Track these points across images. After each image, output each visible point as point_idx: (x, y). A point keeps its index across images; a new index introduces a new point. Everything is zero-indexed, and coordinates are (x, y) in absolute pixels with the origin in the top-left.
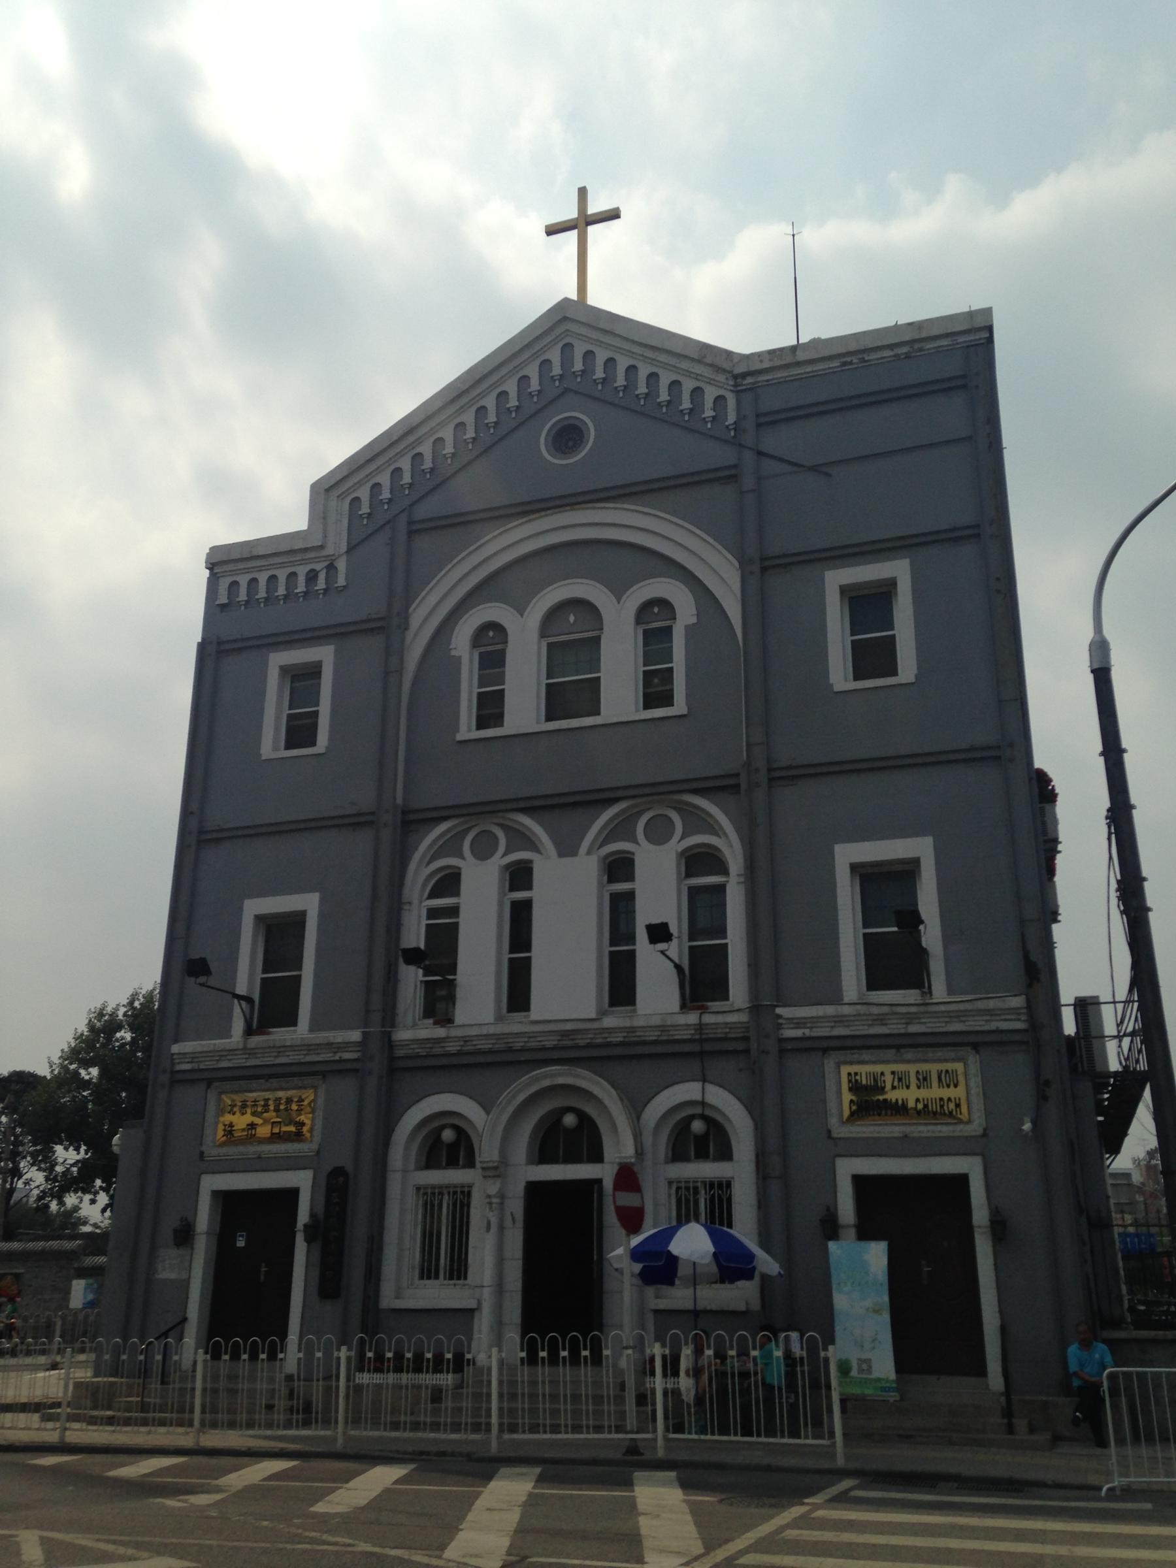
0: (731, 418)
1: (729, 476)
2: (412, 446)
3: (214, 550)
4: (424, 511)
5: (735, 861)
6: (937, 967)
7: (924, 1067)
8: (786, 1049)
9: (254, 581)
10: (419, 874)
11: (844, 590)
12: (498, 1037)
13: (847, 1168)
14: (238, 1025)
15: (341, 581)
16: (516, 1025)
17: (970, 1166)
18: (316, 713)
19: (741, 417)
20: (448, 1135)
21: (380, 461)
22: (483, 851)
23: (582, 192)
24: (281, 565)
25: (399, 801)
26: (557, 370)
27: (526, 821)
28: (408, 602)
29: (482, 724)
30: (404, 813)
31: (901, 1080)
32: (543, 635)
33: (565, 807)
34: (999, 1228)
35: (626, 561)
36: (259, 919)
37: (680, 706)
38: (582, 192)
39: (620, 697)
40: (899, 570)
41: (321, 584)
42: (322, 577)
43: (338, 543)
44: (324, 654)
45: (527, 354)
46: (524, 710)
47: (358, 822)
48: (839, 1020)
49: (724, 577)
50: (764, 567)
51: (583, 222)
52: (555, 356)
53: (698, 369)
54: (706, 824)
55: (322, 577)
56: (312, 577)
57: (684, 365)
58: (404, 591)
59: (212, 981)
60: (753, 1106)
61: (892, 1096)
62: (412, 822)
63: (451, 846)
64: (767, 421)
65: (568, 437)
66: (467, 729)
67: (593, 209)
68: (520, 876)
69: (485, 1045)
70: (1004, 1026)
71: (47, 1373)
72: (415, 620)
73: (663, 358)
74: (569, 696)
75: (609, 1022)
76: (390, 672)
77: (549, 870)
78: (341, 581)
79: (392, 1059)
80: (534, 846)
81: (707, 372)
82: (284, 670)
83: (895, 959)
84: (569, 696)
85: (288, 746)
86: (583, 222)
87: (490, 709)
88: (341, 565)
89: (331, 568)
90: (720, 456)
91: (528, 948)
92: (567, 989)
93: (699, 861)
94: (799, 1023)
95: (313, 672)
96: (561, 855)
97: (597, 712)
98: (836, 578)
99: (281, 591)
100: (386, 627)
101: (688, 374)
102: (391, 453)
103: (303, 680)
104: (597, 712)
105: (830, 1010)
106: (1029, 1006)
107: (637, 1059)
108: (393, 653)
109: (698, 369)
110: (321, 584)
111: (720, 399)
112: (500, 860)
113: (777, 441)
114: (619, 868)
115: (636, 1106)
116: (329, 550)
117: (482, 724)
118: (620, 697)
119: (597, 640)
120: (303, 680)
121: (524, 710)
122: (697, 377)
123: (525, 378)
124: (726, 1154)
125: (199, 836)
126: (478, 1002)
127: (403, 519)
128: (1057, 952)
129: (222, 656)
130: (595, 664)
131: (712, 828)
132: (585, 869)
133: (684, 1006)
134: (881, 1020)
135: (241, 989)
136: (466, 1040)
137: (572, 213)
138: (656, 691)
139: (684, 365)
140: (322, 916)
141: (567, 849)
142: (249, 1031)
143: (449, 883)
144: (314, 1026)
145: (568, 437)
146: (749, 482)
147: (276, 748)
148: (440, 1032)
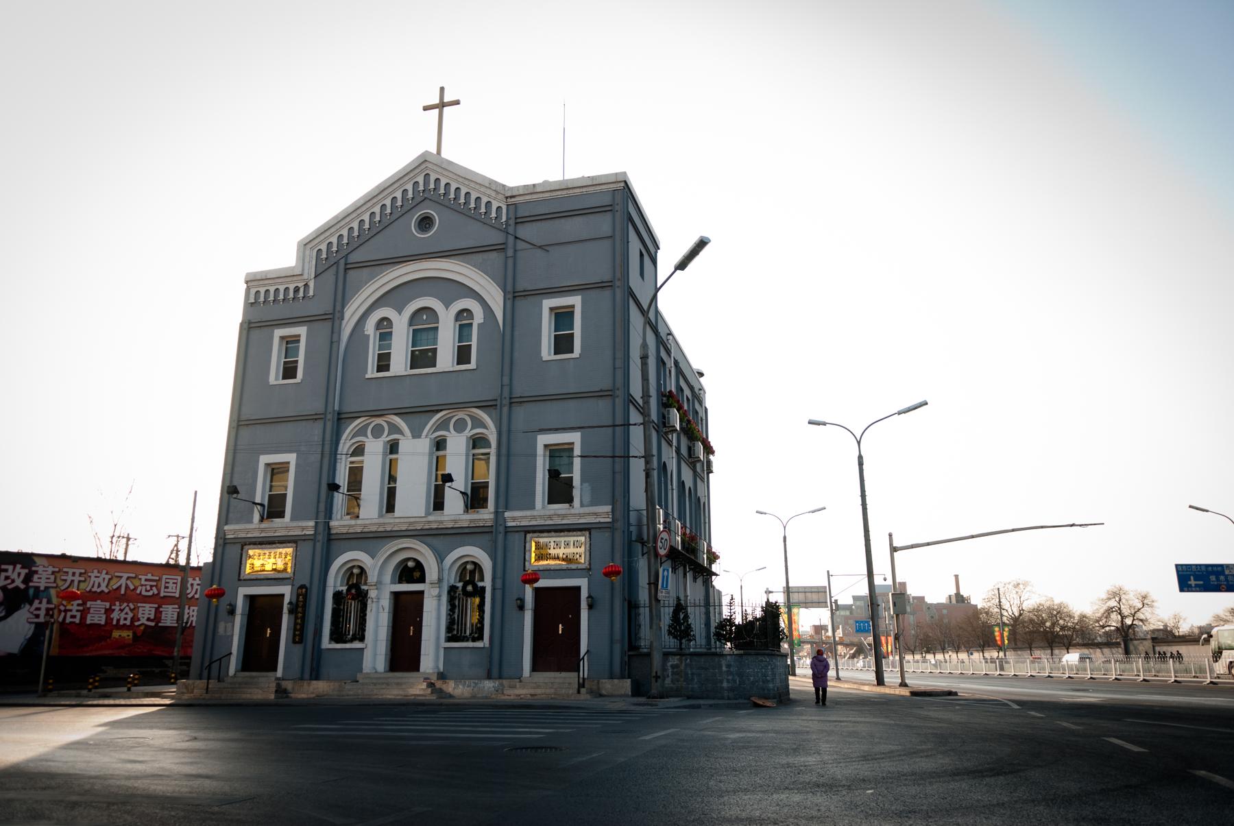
0: (504, 219)
1: (501, 248)
2: (348, 223)
3: (248, 275)
4: (353, 258)
5: (493, 439)
6: (576, 493)
7: (567, 539)
8: (508, 531)
9: (267, 291)
10: (345, 445)
11: (551, 309)
12: (380, 525)
13: (243, 591)
14: (256, 517)
15: (311, 293)
16: (389, 519)
17: (583, 583)
18: (296, 362)
19: (508, 219)
20: (356, 571)
21: (333, 230)
22: (377, 432)
23: (442, 89)
24: (281, 283)
25: (336, 408)
26: (421, 188)
27: (397, 420)
28: (343, 307)
29: (380, 369)
30: (339, 414)
31: (558, 545)
32: (411, 324)
33: (416, 414)
34: (521, 607)
35: (451, 289)
36: (267, 465)
37: (473, 365)
38: (442, 89)
39: (446, 359)
40: (576, 301)
41: (301, 294)
42: (302, 290)
43: (310, 273)
44: (302, 331)
45: (406, 178)
46: (399, 364)
47: (314, 418)
48: (534, 518)
49: (496, 298)
50: (514, 296)
51: (442, 105)
52: (420, 179)
53: (489, 192)
54: (478, 423)
55: (302, 290)
56: (297, 290)
57: (482, 189)
58: (341, 298)
59: (239, 496)
60: (494, 558)
61: (552, 551)
62: (341, 419)
63: (362, 431)
64: (519, 221)
65: (425, 223)
66: (371, 373)
67: (446, 100)
68: (393, 447)
69: (374, 529)
70: (602, 520)
71: (952, 785)
72: (347, 314)
73: (472, 185)
74: (422, 358)
75: (431, 518)
76: (333, 341)
77: (407, 444)
78: (311, 293)
79: (329, 534)
80: (401, 433)
81: (493, 194)
82: (282, 338)
83: (560, 491)
84: (422, 358)
85: (284, 378)
86: (442, 105)
87: (384, 363)
88: (311, 284)
89: (306, 285)
90: (495, 238)
91: (395, 481)
92: (413, 502)
93: (477, 442)
94: (514, 519)
95: (295, 339)
96: (414, 437)
97: (434, 366)
98: (548, 303)
99: (281, 297)
100: (333, 317)
101: (485, 194)
102: (338, 226)
103: (290, 343)
104: (434, 366)
105: (528, 513)
106: (613, 511)
107: (442, 537)
108: (335, 332)
109: (489, 192)
110: (301, 294)
111: (499, 208)
112: (385, 438)
113: (526, 231)
114: (440, 445)
115: (440, 558)
116: (305, 276)
117: (380, 369)
118: (446, 359)
119: (437, 328)
120: (290, 343)
121: (399, 364)
122: (489, 196)
123: (405, 190)
124: (422, 580)
125: (240, 423)
126: (370, 508)
127: (342, 262)
128: (24, 551)
129: (254, 328)
130: (435, 341)
131: (485, 427)
132: (423, 445)
133: (467, 510)
134: (550, 517)
135: (258, 500)
136: (365, 526)
137: (437, 101)
138: (463, 355)
139: (482, 189)
140: (297, 465)
141: (416, 434)
142: (262, 519)
143: (359, 451)
144: (292, 519)
145: (425, 223)
146: (510, 253)
147: (276, 379)
148: (353, 522)
